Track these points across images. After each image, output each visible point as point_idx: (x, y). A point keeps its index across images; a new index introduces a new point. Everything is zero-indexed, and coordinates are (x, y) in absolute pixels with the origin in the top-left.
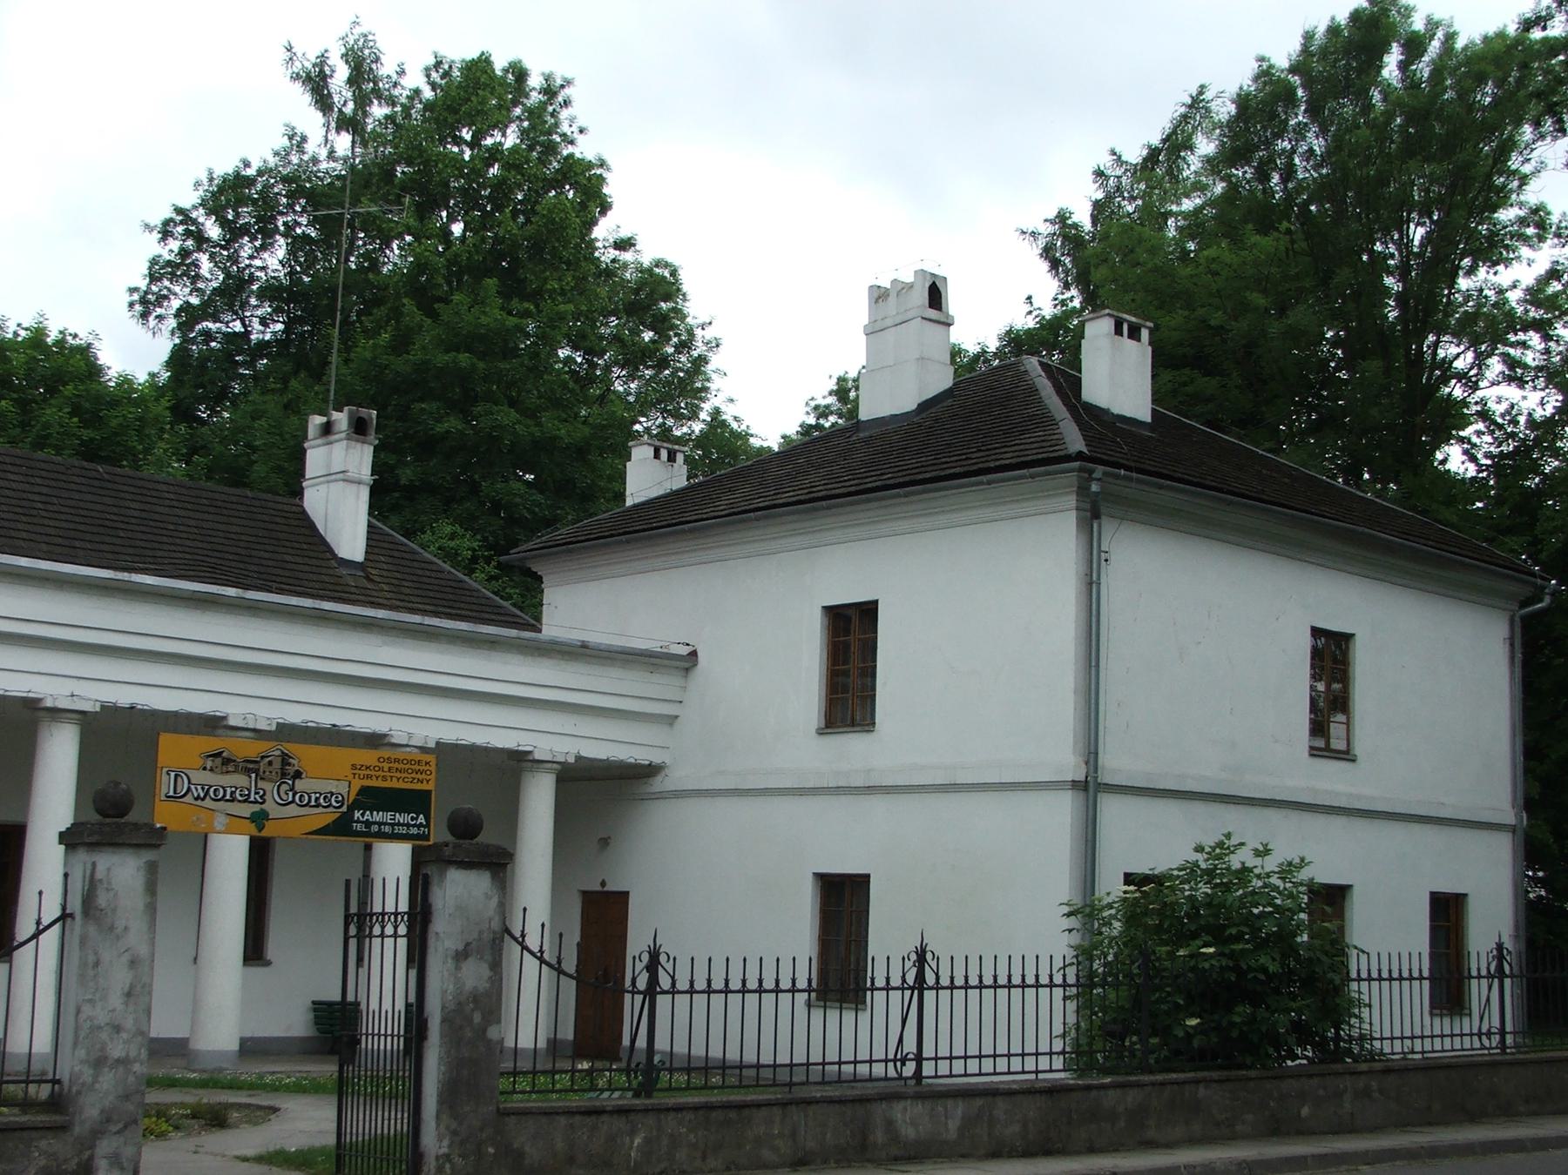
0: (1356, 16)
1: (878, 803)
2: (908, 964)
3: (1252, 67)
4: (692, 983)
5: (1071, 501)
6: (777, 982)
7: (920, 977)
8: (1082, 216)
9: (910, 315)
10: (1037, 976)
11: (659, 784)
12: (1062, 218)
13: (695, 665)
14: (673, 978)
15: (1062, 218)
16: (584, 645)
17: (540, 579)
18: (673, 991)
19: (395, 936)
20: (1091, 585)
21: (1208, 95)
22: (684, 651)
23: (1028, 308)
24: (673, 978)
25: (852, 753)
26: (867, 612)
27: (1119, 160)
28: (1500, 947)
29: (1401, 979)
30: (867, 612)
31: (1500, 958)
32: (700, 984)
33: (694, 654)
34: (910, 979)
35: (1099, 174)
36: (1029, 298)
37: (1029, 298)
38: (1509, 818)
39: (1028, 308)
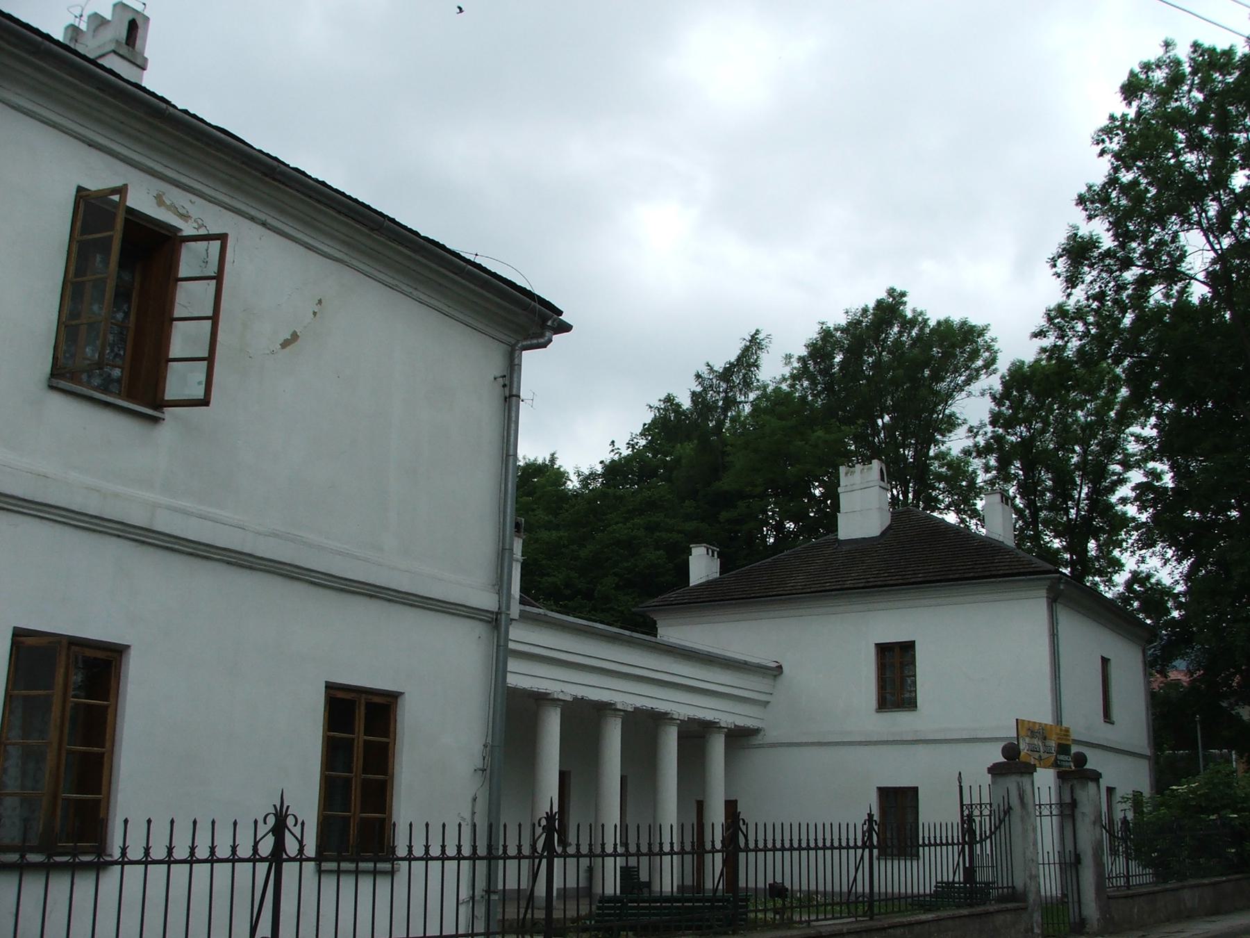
0: (880, 303)
1: (920, 748)
2: (539, 830)
3: (817, 328)
4: (147, 850)
5: (1044, 593)
6: (234, 848)
7: (279, 846)
8: (686, 403)
9: (872, 484)
10: (427, 847)
11: (758, 740)
12: (669, 399)
13: (782, 673)
14: (301, 842)
15: (669, 399)
16: (746, 663)
17: (655, 623)
18: (747, 850)
19: (1051, 815)
20: (1054, 635)
21: (761, 336)
22: (774, 665)
23: (611, 448)
24: (301, 842)
25: (900, 722)
26: (908, 648)
27: (711, 369)
28: (870, 816)
29: (848, 847)
30: (908, 648)
31: (279, 830)
32: (158, 852)
33: (780, 667)
34: (266, 848)
35: (698, 376)
36: (613, 442)
37: (613, 442)
38: (1148, 752)
39: (611, 448)
